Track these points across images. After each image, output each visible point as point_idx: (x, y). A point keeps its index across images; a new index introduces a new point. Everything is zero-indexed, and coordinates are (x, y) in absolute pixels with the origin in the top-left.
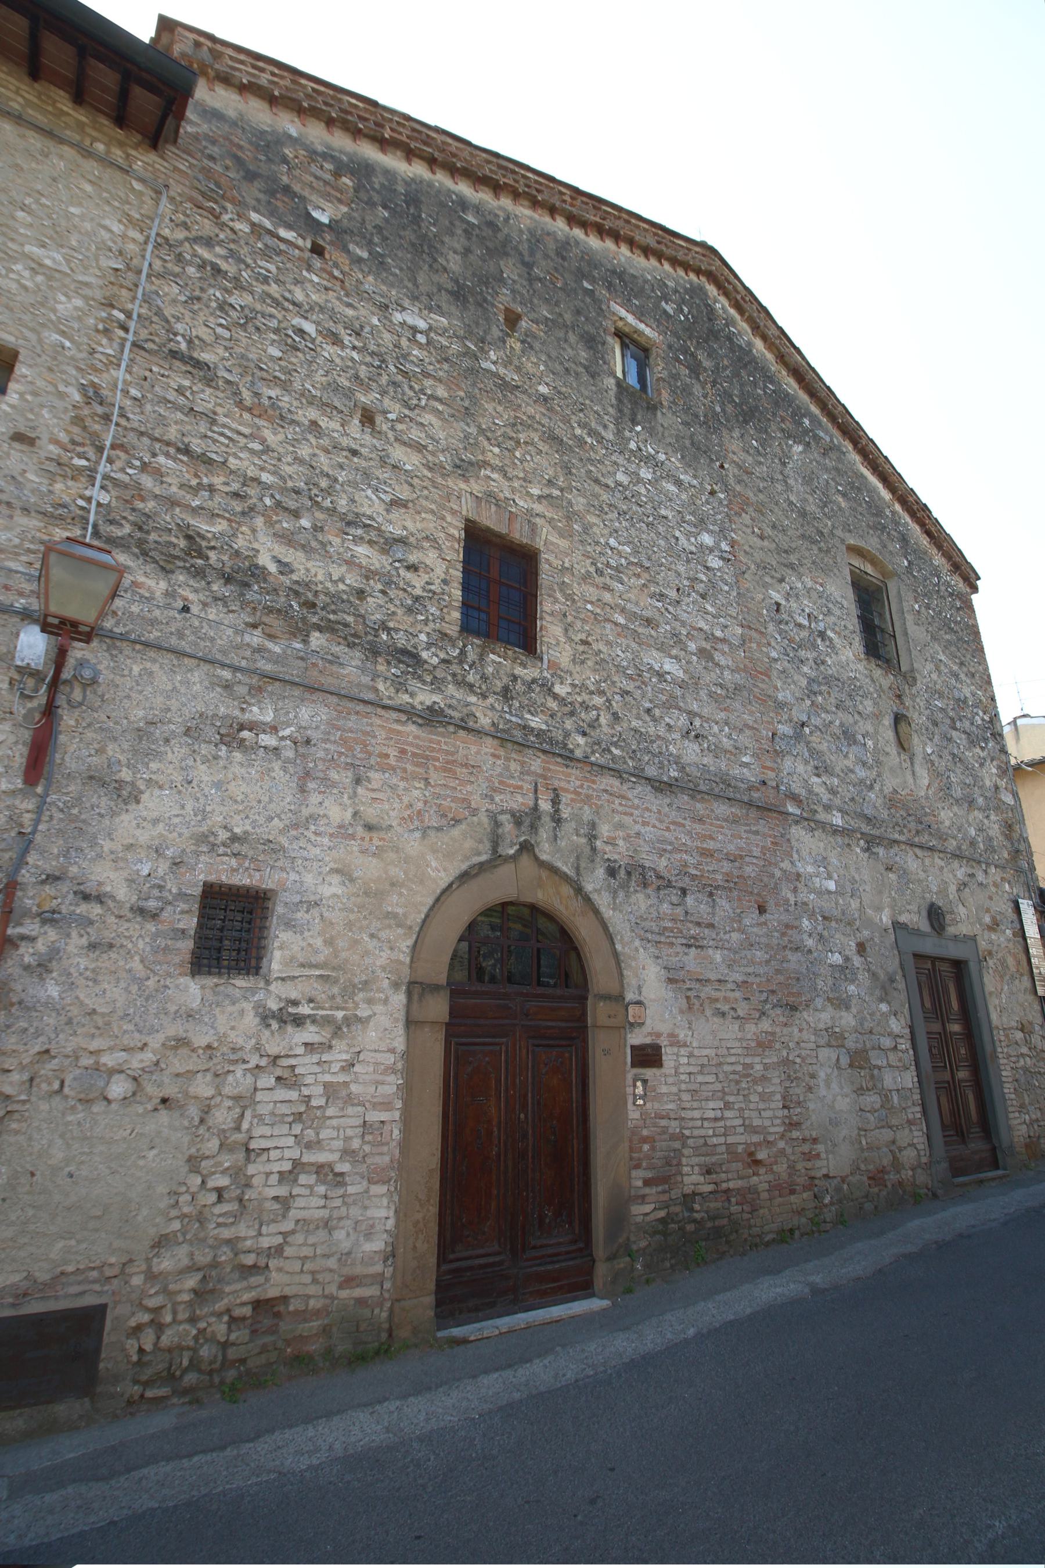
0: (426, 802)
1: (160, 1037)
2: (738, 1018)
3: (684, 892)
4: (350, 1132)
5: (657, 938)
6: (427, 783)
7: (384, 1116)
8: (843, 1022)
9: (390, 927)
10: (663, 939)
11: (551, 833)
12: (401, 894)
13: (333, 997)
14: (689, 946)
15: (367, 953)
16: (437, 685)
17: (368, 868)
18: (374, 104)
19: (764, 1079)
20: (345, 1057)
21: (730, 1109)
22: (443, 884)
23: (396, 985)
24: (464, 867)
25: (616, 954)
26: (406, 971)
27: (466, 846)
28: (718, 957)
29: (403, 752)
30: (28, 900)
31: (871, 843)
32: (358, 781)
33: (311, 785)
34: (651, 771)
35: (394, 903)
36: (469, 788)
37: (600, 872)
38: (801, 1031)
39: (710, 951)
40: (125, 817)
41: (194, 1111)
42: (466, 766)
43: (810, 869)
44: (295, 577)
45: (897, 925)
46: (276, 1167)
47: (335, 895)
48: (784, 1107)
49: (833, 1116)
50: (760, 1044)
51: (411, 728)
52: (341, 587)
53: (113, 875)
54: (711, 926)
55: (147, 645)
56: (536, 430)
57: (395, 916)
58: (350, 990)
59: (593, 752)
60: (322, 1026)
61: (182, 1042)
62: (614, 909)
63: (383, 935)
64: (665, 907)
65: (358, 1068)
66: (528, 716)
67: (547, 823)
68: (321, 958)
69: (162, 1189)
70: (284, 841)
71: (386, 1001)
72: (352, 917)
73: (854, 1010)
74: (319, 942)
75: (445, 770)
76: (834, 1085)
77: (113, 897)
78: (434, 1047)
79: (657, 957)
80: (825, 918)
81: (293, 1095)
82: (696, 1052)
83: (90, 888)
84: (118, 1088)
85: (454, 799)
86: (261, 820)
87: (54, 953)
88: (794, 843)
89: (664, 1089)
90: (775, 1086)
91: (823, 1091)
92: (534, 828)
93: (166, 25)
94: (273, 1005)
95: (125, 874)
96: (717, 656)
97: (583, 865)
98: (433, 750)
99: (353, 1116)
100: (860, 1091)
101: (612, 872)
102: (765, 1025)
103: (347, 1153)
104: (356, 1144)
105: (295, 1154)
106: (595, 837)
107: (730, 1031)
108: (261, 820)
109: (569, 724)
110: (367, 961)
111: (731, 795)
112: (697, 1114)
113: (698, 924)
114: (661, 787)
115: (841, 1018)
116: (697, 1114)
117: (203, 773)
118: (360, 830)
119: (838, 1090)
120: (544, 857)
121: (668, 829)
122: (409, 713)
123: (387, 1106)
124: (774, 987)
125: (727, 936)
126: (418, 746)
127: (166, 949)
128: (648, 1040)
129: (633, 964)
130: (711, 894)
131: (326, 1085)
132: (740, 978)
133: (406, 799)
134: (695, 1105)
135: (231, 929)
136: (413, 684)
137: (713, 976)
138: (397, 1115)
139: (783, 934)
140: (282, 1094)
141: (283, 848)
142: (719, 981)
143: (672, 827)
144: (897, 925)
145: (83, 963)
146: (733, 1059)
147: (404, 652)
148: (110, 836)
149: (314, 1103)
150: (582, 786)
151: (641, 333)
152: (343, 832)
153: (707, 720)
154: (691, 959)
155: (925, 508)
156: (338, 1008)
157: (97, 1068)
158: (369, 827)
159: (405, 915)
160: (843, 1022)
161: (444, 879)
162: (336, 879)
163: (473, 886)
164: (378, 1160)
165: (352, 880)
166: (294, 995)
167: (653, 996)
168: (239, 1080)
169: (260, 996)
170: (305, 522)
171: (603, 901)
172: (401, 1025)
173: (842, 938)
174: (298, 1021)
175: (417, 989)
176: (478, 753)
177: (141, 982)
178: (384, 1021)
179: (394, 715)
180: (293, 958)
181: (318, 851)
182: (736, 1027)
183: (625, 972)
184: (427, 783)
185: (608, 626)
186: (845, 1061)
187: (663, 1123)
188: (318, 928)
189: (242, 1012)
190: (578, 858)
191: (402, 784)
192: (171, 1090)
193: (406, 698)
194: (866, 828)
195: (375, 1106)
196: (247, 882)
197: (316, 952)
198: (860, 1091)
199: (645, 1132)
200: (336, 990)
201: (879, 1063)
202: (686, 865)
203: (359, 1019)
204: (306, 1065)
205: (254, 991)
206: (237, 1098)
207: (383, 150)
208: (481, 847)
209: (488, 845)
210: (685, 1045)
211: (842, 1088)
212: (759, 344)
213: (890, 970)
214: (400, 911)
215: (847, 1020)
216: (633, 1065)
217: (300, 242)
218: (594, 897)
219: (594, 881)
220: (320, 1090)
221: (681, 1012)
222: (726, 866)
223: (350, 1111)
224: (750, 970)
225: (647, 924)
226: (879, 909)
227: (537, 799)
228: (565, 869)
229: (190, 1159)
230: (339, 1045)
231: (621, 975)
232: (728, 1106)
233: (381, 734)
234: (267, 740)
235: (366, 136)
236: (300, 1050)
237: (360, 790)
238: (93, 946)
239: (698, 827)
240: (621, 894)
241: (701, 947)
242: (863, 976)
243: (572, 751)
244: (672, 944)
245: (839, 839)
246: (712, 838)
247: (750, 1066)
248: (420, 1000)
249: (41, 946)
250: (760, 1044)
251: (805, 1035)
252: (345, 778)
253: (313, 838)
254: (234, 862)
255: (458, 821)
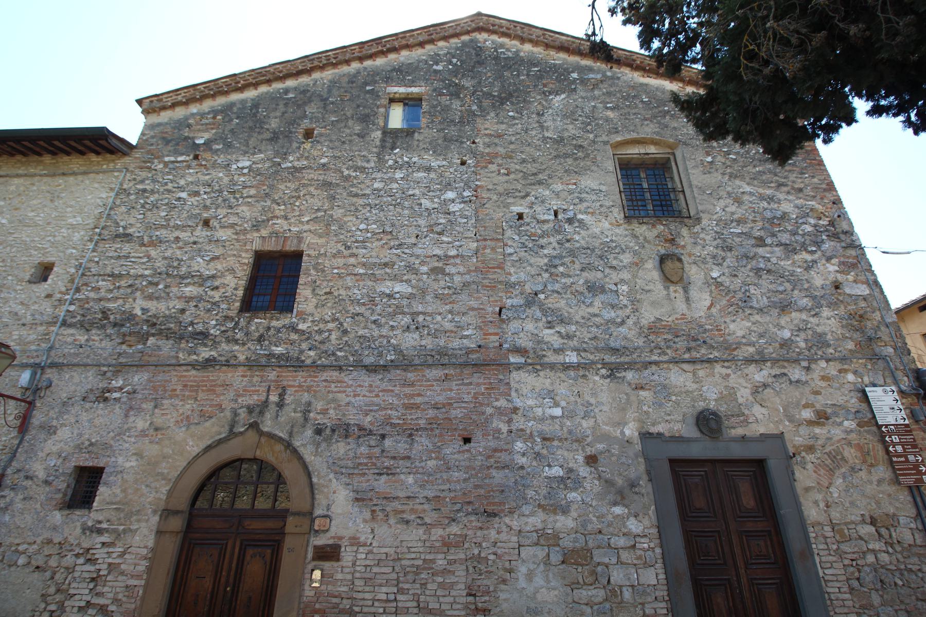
0: (192, 411)
1: (41, 538)
2: (425, 524)
3: (383, 437)
4: (118, 590)
5: (351, 471)
6: (196, 399)
7: (135, 582)
8: (558, 525)
9: (158, 480)
10: (356, 471)
11: (274, 414)
12: (168, 462)
13: (120, 519)
14: (381, 474)
15: (142, 495)
16: (215, 344)
17: (152, 450)
18: (235, 75)
19: (445, 572)
20: (120, 550)
21: (403, 594)
22: (194, 454)
23: (155, 512)
24: (209, 443)
25: (311, 485)
26: (163, 503)
27: (214, 429)
28: (410, 480)
29: (185, 386)
30: (8, 481)
31: (613, 371)
32: (156, 407)
33: (132, 413)
34: (369, 360)
35: (163, 468)
36: (222, 398)
37: (309, 433)
38: (498, 533)
39: (402, 477)
40: (49, 442)
41: (48, 574)
42: (223, 386)
43: (530, 402)
44: (149, 314)
45: (646, 436)
46: (78, 604)
47: (132, 467)
48: (469, 595)
49: (533, 605)
50: (445, 544)
51: (194, 372)
52: (173, 310)
53: (39, 467)
54: (409, 458)
55: (74, 365)
56: (311, 185)
57: (162, 474)
58: (129, 515)
59: (320, 358)
60: (111, 533)
61: (49, 542)
62: (315, 456)
63: (153, 485)
64: (363, 449)
65: (127, 556)
66: (274, 348)
67: (273, 408)
68: (118, 499)
69: (29, 608)
70: (112, 442)
71: (147, 521)
72: (138, 477)
73: (574, 514)
74: (118, 491)
75: (208, 390)
76: (539, 581)
77: (37, 477)
78: (171, 546)
79: (348, 484)
80: (545, 439)
81: (92, 568)
82: (375, 550)
83: (29, 474)
84: (22, 561)
85: (211, 406)
86: (105, 434)
87: (12, 502)
88: (512, 384)
89: (339, 576)
90: (460, 575)
91: (522, 583)
92: (261, 413)
93: (150, 105)
94: (90, 524)
95: (43, 466)
96: (448, 269)
97: (295, 430)
98: (204, 381)
99: (122, 581)
100: (574, 585)
101: (318, 432)
102: (455, 529)
103: (116, 601)
104: (120, 596)
105: (88, 598)
106: (309, 411)
107: (414, 536)
108: (105, 434)
109: (304, 346)
110: (142, 499)
111: (446, 361)
112: (367, 596)
113: (394, 458)
114: (372, 369)
115: (556, 521)
116: (367, 596)
117: (84, 417)
118: (151, 431)
119: (542, 583)
120: (266, 429)
121: (377, 396)
122: (193, 365)
123: (139, 577)
124: (472, 499)
125: (423, 464)
126: (195, 381)
127: (51, 498)
128: (331, 542)
129: (326, 490)
130: (411, 435)
131: (110, 564)
132: (431, 494)
133: (181, 411)
134: (367, 589)
135: (85, 484)
136: (201, 349)
137: (401, 494)
138: (143, 582)
139: (489, 457)
140: (88, 567)
141: (111, 446)
142: (409, 497)
143: (380, 394)
144: (646, 436)
145: (20, 506)
146: (413, 556)
147: (201, 333)
148: (42, 451)
149: (101, 573)
150: (305, 382)
151: (412, 93)
152: (143, 434)
153: (430, 315)
154: (382, 484)
155: (378, 41)
156: (121, 525)
157: (17, 551)
158: (156, 429)
159: (168, 473)
160: (558, 525)
161: (196, 450)
162: (134, 458)
163: (213, 452)
164: (129, 606)
165: (142, 458)
166: (100, 518)
167: (340, 511)
168: (69, 560)
169: (85, 519)
170: (161, 286)
171: (307, 454)
172: (153, 533)
173: (566, 453)
174: (100, 532)
175: (167, 513)
176: (233, 377)
177: (38, 513)
178: (145, 531)
179: (184, 368)
180: (104, 500)
181: (127, 445)
182: (421, 531)
183: (317, 496)
184: (196, 399)
185: (349, 278)
186: (556, 558)
187: (335, 600)
188: (119, 484)
189: (75, 527)
190: (292, 426)
191: (181, 403)
192: (40, 563)
193: (195, 357)
194: (609, 358)
195: (132, 576)
196: (91, 464)
197: (116, 496)
198: (574, 585)
199: (317, 606)
200: (122, 515)
201: (606, 560)
202: (390, 418)
203: (131, 530)
204: (100, 553)
205: (83, 516)
206: (67, 568)
207: (242, 92)
208: (222, 430)
209: (227, 428)
210: (365, 545)
211: (548, 581)
212: (528, 47)
213: (633, 476)
214: (166, 471)
215: (565, 523)
216: (314, 559)
217: (188, 158)
218: (301, 450)
219: (303, 441)
220: (105, 566)
221: (365, 521)
222: (431, 413)
223: (120, 578)
224: (446, 487)
225: (342, 463)
226: (622, 423)
227: (268, 396)
228: (281, 435)
229: (43, 595)
230: (119, 544)
231: (313, 498)
232: (401, 591)
233: (174, 380)
234: (116, 395)
235: (233, 91)
236: (99, 546)
237: (156, 410)
238: (25, 499)
239: (408, 390)
240: (324, 445)
241: (394, 474)
242: (592, 485)
243: (303, 361)
244: (365, 474)
245: (572, 373)
246: (419, 395)
247: (433, 561)
248: (165, 520)
249: (8, 499)
250: (445, 544)
251: (503, 537)
252: (148, 406)
253: (126, 439)
254: (87, 456)
255: (211, 417)
